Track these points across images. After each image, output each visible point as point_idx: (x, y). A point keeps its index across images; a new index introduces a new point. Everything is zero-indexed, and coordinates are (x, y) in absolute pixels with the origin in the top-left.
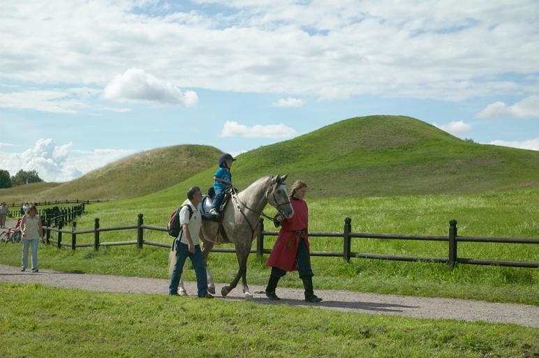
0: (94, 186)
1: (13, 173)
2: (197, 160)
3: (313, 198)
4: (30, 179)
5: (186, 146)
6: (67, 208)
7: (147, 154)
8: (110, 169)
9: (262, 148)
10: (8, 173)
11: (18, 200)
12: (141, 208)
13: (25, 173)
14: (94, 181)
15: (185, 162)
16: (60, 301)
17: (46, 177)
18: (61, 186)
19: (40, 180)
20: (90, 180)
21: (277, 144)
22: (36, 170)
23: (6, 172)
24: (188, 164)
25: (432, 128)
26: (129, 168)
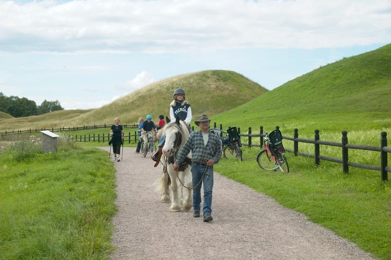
0: (127, 111)
1: (39, 103)
2: (225, 84)
3: (230, 175)
4: (51, 108)
5: (211, 71)
6: (101, 135)
7: (175, 80)
8: (139, 95)
9: (345, 60)
10: (35, 103)
11: (56, 125)
12: (38, 171)
13: (49, 103)
14: (126, 106)
15: (213, 86)
16: (106, 220)
17: (66, 106)
18: (91, 112)
19: (63, 109)
20: (122, 105)
21: (229, 72)
22: (59, 100)
23: (33, 102)
24: (217, 87)
25: (282, 88)
26: (159, 93)
